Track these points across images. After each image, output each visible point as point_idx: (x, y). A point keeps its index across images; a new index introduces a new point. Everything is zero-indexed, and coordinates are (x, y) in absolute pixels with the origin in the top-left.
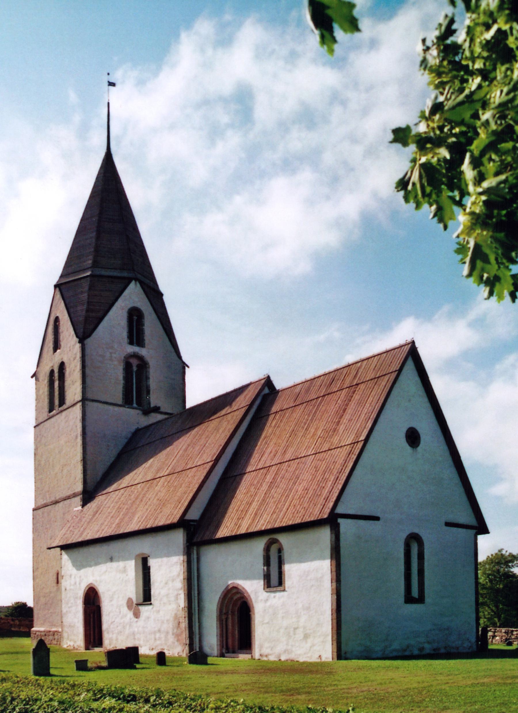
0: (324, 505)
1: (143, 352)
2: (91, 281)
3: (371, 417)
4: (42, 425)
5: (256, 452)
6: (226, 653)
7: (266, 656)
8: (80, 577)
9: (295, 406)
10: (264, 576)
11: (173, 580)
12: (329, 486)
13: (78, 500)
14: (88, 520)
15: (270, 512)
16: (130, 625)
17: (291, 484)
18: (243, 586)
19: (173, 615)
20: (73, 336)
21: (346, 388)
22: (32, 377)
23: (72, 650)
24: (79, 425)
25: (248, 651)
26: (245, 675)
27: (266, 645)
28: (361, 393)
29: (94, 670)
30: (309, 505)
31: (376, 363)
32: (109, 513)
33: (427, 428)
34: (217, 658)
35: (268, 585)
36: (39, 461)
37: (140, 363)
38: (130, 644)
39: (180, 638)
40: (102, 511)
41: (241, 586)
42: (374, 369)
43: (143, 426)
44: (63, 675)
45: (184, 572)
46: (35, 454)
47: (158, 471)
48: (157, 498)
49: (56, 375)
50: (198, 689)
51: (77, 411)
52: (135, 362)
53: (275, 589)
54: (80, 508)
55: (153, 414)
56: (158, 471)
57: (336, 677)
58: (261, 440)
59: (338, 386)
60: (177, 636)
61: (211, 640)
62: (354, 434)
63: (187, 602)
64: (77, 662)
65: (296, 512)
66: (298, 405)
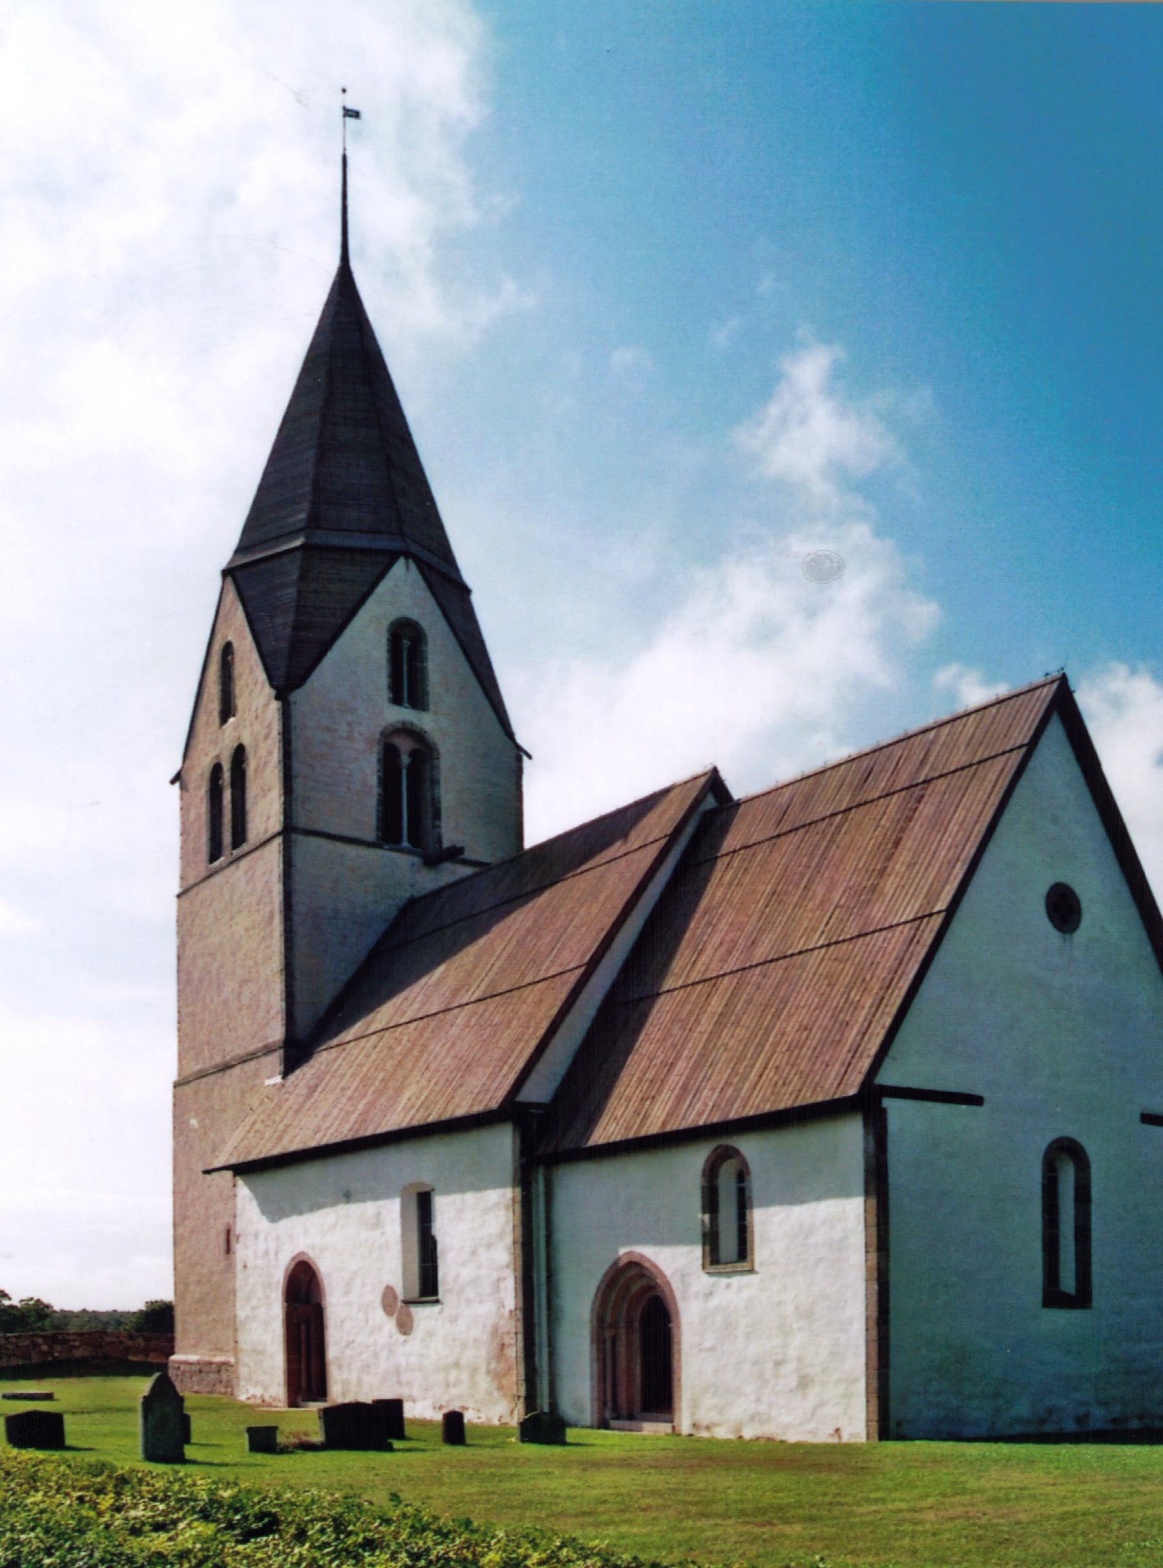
0: (850, 1064)
1: (425, 721)
2: (303, 559)
3: (963, 857)
4: (195, 890)
5: (684, 944)
6: (614, 1419)
7: (708, 1428)
8: (278, 1238)
9: (779, 836)
10: (704, 1235)
11: (489, 1246)
12: (861, 1019)
13: (275, 1061)
14: (295, 1107)
15: (719, 1082)
16: (391, 1351)
17: (769, 1017)
18: (653, 1259)
19: (489, 1329)
20: (263, 684)
21: (902, 790)
22: (173, 782)
23: (258, 1406)
24: (277, 888)
25: (666, 1416)
26: (652, 1471)
27: (709, 1401)
28: (937, 801)
29: (291, 1452)
30: (814, 1064)
31: (972, 731)
32: (344, 1089)
33: (1096, 887)
34: (589, 1431)
35: (714, 1258)
36: (189, 973)
37: (416, 746)
38: (387, 1393)
39: (504, 1381)
40: (326, 1085)
41: (649, 1260)
42: (968, 745)
43: (423, 893)
44: (215, 1461)
45: (514, 1227)
46: (179, 958)
47: (456, 992)
48: (453, 1053)
49: (227, 775)
50: (531, 1502)
51: (273, 855)
52: (405, 745)
53: (729, 1268)
54: (278, 1079)
55: (448, 866)
56: (456, 992)
57: (879, 1480)
58: (697, 916)
59: (883, 785)
60: (497, 1377)
61: (578, 1388)
62: (922, 897)
63: (520, 1296)
64: (250, 1430)
65: (781, 1082)
66: (785, 834)
